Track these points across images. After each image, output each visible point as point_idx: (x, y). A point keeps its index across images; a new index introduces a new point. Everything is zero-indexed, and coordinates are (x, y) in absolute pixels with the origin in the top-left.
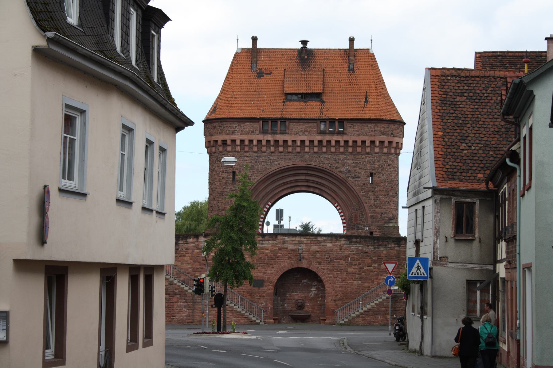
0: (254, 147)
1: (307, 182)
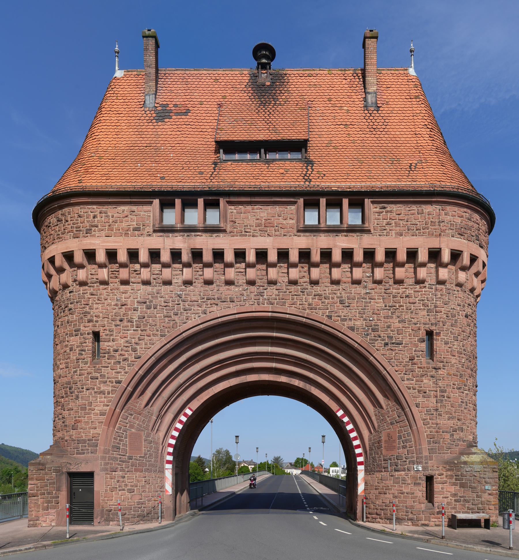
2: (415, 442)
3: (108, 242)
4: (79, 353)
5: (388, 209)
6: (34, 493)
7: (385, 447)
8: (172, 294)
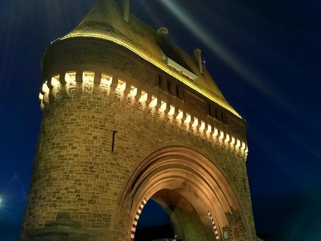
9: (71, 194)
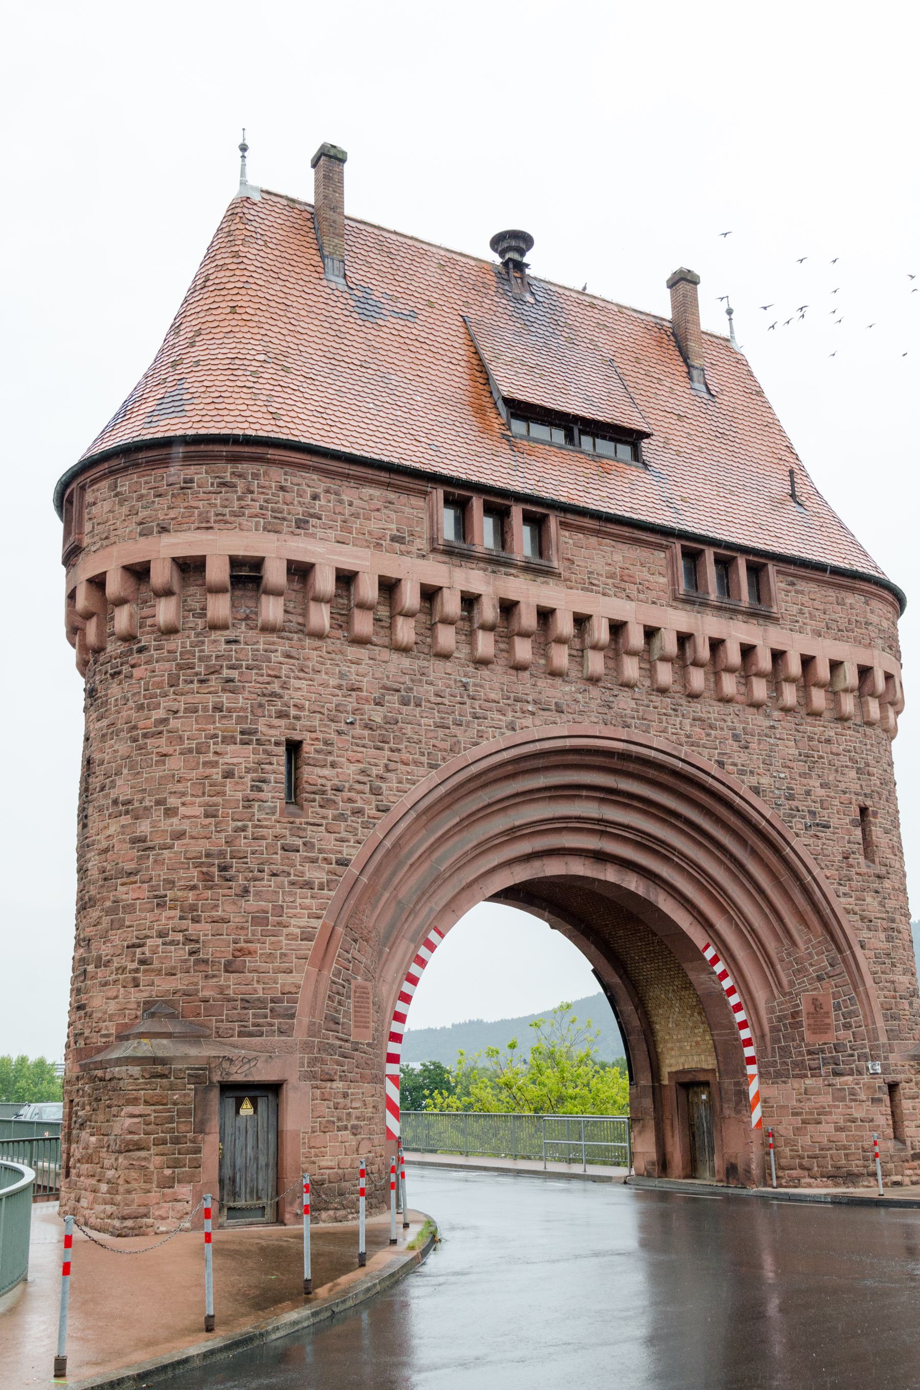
0: (400, 620)
1: (602, 833)
2: (865, 1016)
3: (340, 554)
4: (252, 786)
5: (798, 587)
6: (140, 1140)
7: (809, 1025)
8: (450, 679)
9: (175, 949)
